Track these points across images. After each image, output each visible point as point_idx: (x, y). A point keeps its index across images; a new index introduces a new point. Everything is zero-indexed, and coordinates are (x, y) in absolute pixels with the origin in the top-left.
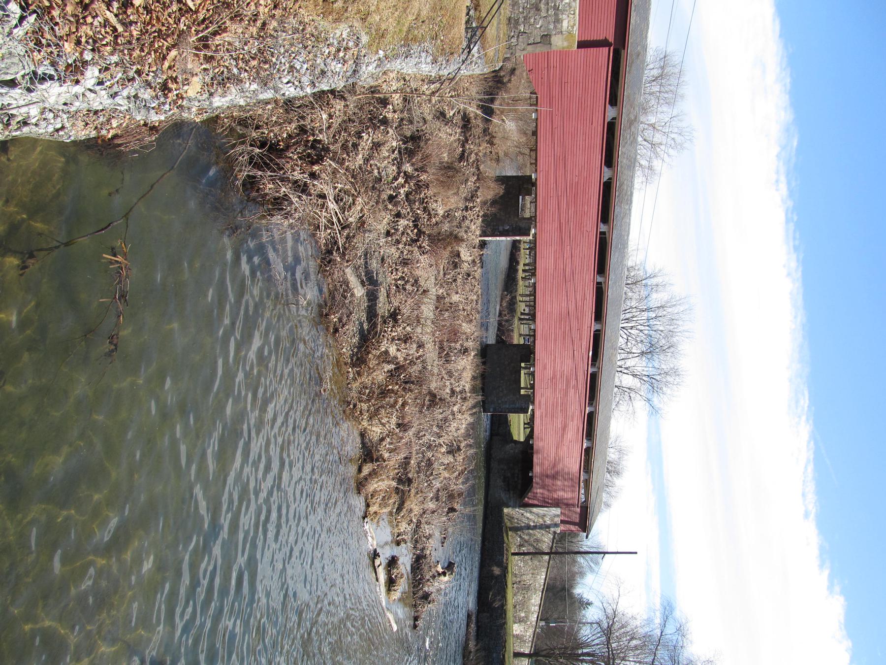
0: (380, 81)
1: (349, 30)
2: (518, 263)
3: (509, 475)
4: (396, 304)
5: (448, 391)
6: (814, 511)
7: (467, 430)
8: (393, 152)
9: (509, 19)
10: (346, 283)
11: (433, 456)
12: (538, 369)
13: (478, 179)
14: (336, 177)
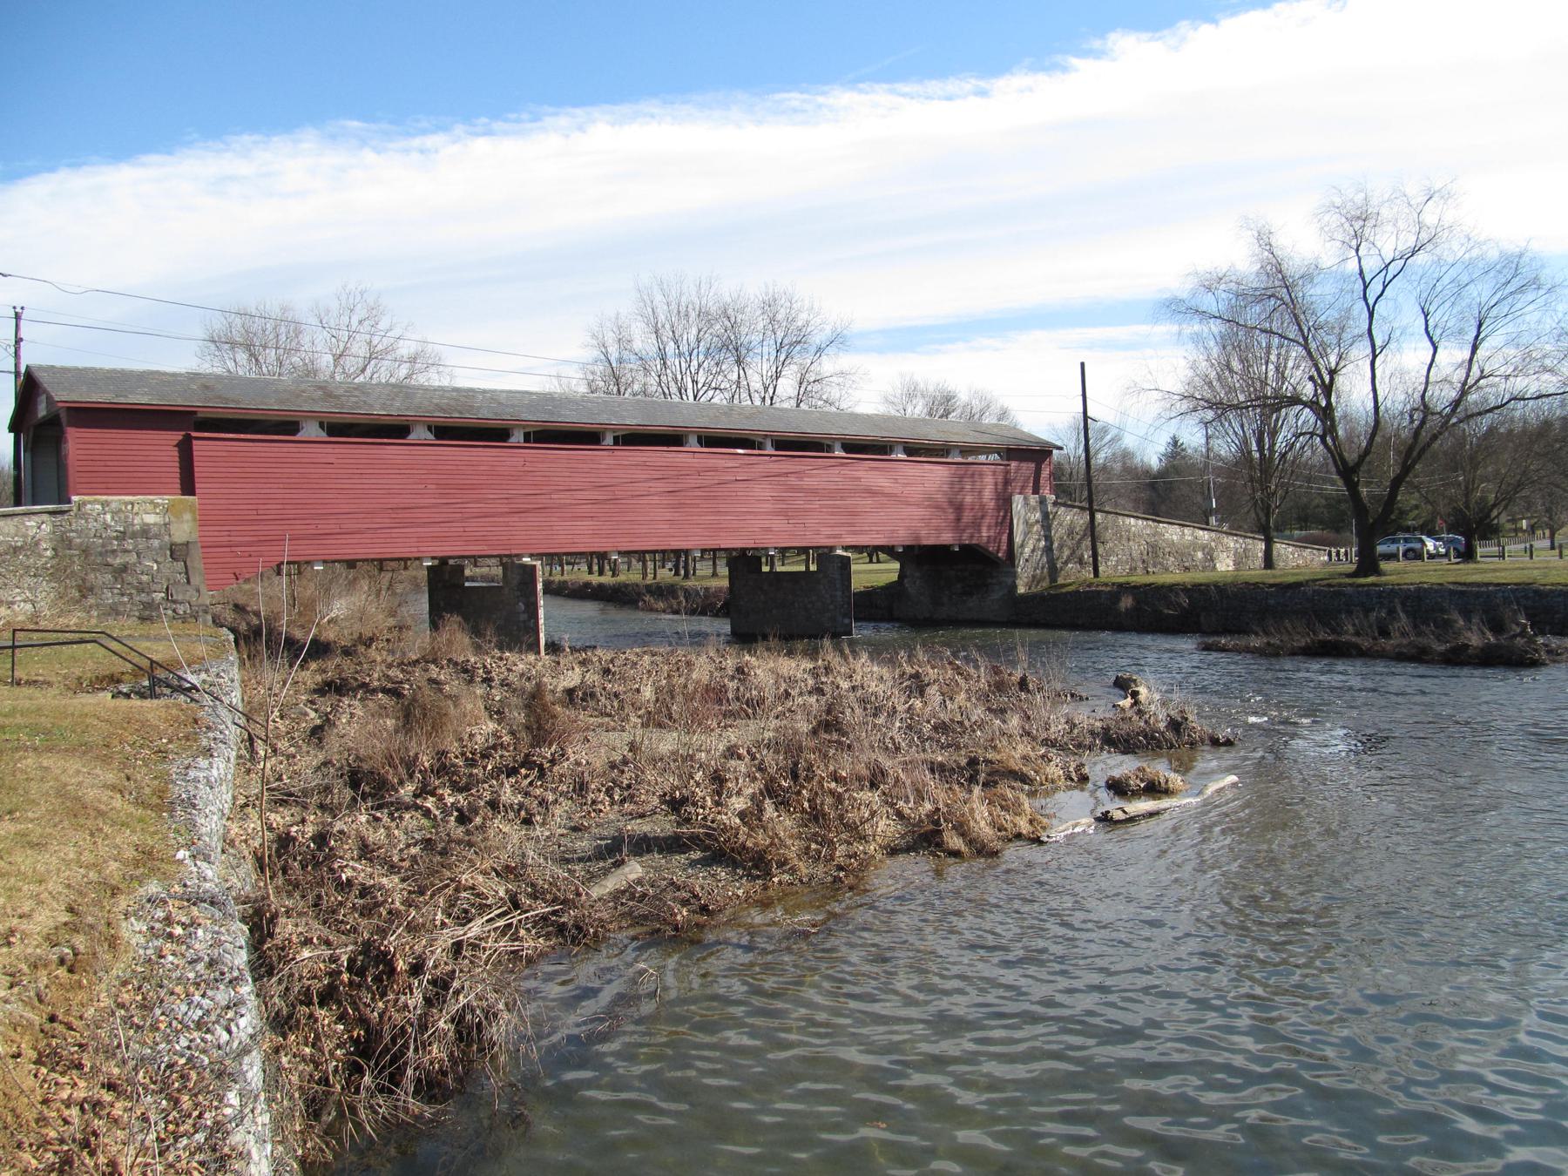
0: (246, 853)
1: (133, 919)
2: (587, 585)
3: (959, 586)
4: (656, 801)
5: (813, 700)
6: (973, 81)
7: (881, 663)
8: (377, 819)
9: (142, 619)
10: (617, 895)
11: (928, 722)
12: (772, 541)
13: (434, 661)
14: (424, 925)
